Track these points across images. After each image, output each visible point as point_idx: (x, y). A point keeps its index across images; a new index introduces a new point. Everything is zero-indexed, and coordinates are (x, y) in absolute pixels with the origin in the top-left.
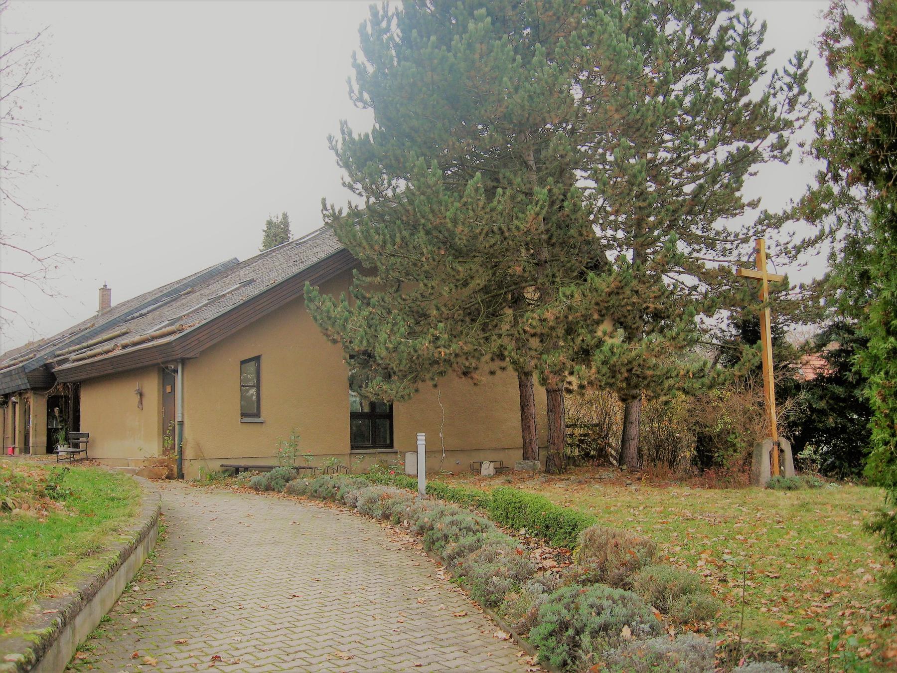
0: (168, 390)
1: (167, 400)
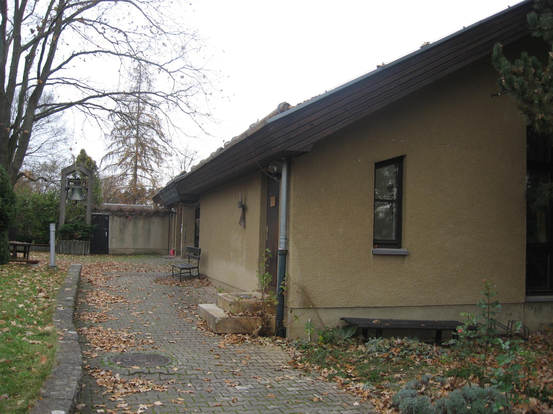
0: (273, 204)
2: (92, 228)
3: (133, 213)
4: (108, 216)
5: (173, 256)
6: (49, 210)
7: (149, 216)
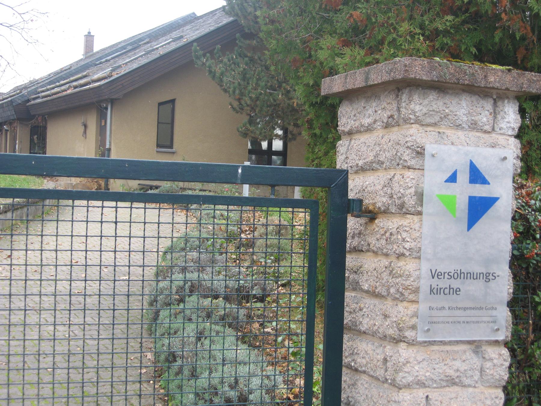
0: (103, 124)
1: (101, 131)
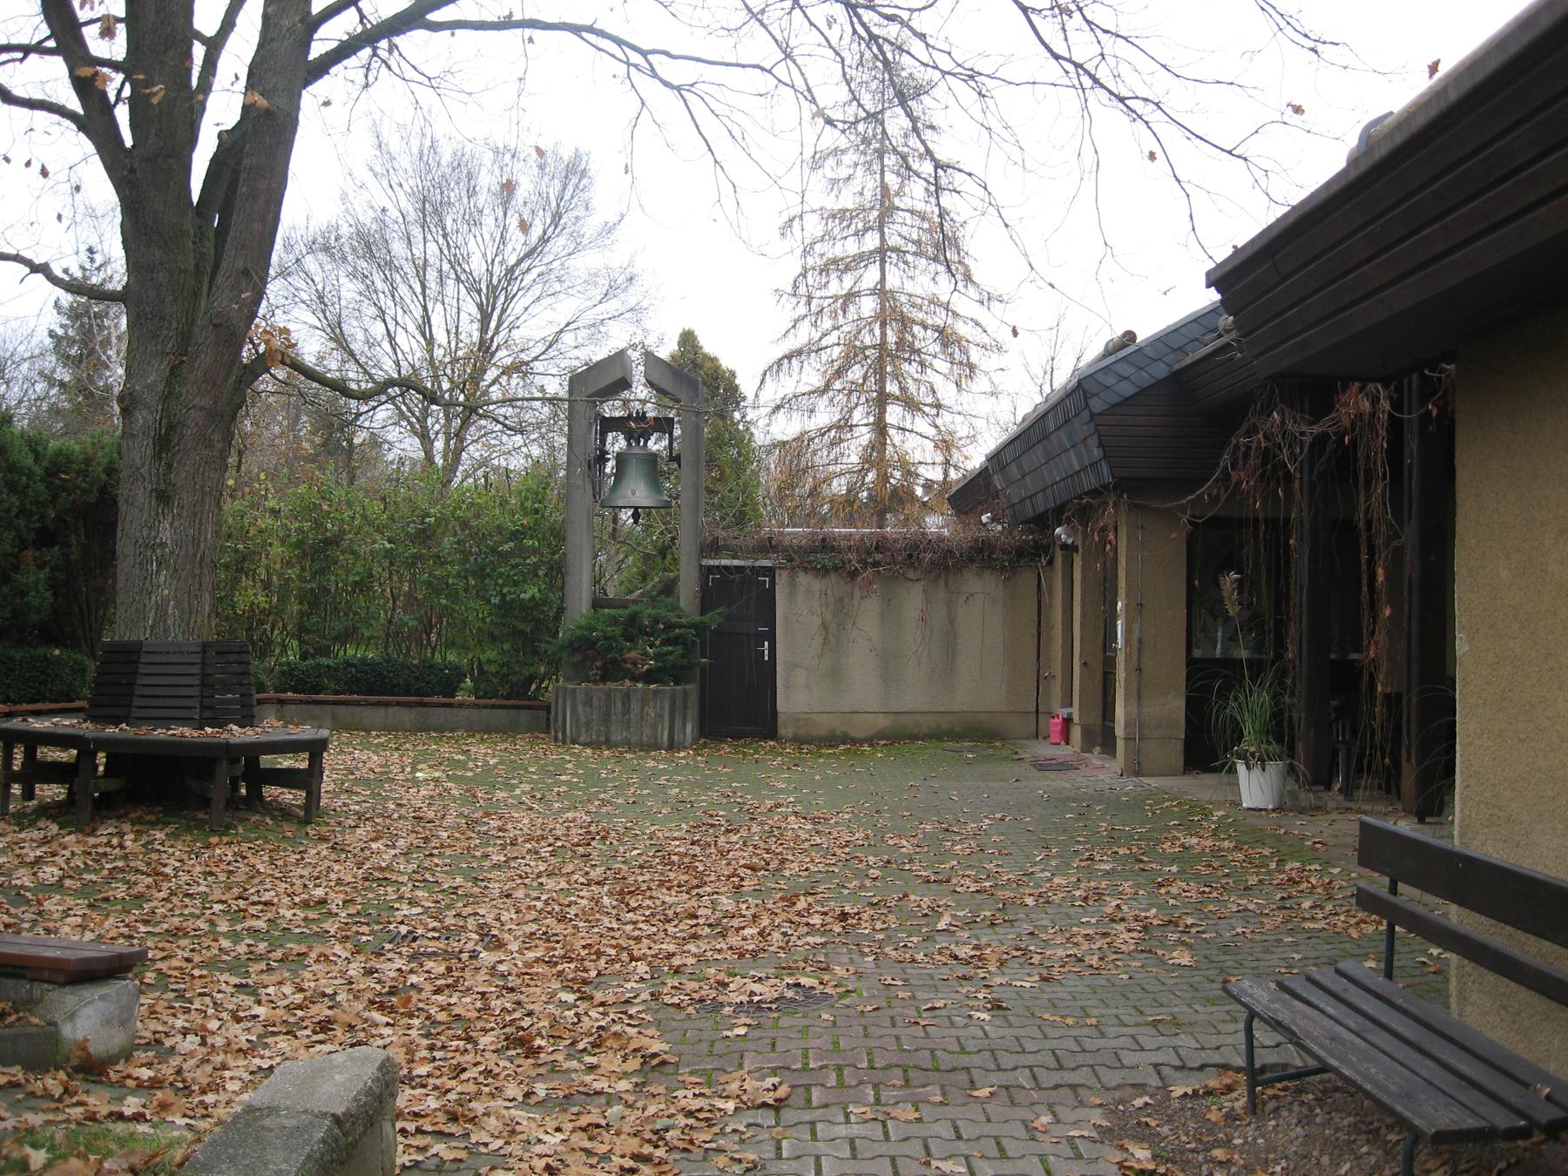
2: (700, 628)
3: (878, 557)
4: (770, 572)
5: (1062, 752)
6: (521, 551)
7: (947, 568)
